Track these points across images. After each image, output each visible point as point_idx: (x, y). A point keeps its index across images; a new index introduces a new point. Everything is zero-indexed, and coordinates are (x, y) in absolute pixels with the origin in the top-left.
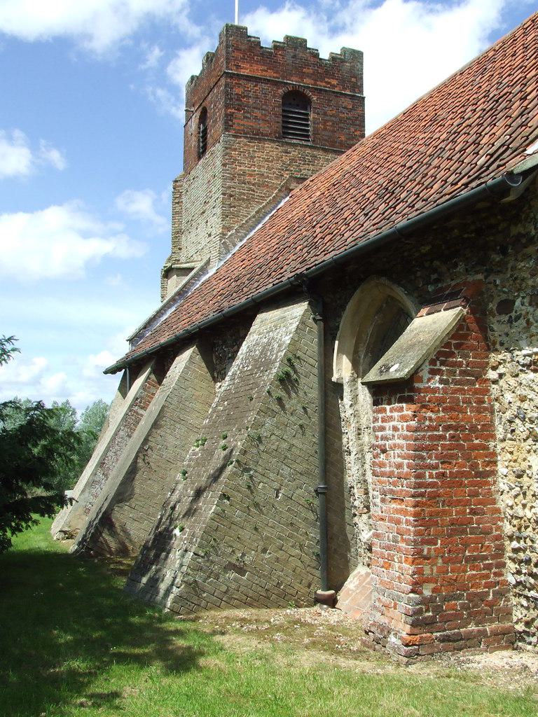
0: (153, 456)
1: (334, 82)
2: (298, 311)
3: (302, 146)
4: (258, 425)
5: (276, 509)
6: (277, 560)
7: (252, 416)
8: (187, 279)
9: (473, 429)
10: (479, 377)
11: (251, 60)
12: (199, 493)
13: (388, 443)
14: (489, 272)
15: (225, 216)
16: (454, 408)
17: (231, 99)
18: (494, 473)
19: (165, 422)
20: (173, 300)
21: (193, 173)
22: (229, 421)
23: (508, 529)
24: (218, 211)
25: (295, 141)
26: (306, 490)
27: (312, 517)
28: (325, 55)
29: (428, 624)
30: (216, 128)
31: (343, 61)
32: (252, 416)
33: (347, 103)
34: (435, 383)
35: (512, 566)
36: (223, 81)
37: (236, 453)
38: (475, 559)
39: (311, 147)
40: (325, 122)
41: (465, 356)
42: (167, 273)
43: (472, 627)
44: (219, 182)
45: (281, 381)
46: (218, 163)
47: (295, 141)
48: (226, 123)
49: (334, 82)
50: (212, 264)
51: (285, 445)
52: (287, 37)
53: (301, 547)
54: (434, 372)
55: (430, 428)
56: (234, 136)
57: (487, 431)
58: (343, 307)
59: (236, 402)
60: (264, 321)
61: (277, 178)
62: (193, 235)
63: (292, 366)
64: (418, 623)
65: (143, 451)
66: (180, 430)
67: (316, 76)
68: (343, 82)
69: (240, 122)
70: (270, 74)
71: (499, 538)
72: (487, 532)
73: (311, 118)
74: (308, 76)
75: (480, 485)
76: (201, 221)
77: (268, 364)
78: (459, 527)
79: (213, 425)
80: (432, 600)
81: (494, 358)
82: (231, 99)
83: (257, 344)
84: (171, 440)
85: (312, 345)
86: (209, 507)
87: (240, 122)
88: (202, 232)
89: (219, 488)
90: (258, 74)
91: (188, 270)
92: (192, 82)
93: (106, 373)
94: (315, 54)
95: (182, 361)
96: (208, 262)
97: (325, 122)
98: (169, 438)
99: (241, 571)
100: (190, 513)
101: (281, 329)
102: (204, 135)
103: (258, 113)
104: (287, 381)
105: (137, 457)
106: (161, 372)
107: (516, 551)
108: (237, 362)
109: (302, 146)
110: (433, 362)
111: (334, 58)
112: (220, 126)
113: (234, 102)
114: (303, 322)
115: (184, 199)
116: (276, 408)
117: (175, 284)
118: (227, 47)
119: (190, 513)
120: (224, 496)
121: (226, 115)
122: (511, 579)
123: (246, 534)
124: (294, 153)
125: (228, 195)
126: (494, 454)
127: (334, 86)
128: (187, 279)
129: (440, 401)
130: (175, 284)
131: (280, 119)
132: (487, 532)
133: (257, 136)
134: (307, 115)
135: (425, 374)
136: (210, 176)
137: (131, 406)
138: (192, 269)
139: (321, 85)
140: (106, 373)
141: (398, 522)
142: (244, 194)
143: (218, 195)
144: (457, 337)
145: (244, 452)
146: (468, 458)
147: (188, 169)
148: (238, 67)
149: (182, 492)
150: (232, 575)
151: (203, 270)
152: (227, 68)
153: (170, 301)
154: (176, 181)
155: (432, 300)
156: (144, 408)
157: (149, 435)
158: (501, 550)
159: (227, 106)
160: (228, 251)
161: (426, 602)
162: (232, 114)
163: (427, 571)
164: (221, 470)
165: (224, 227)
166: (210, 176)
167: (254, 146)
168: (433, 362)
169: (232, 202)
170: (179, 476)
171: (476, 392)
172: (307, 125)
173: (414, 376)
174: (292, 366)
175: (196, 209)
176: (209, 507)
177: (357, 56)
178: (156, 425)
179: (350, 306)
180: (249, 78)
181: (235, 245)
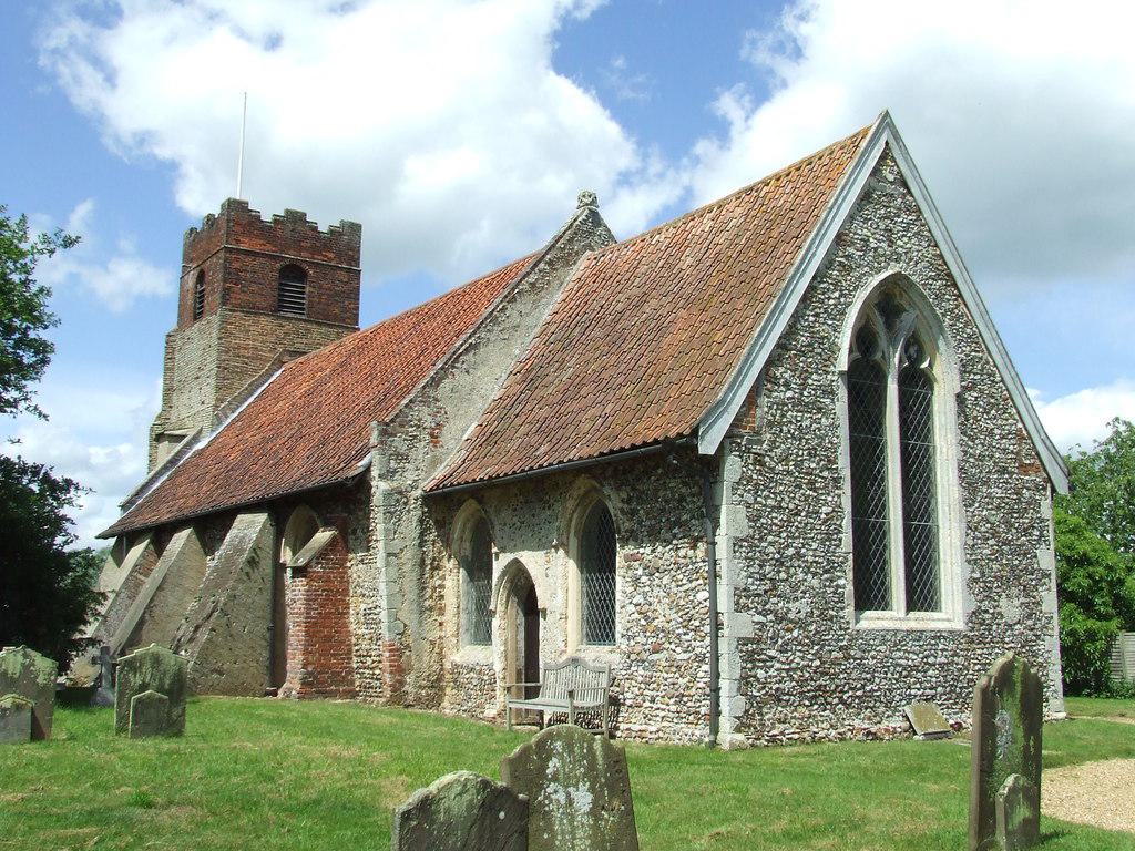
0: (157, 611)
1: (332, 255)
2: (262, 518)
3: (296, 319)
4: (234, 588)
6: (243, 668)
7: (231, 583)
8: (179, 446)
9: (338, 591)
10: (342, 566)
11: (250, 235)
12: (197, 628)
13: (297, 598)
14: (350, 513)
15: (219, 388)
16: (328, 580)
17: (230, 273)
18: (348, 613)
19: (167, 586)
20: (165, 468)
21: (187, 332)
22: (217, 586)
23: (354, 640)
24: (212, 382)
25: (289, 315)
26: (262, 627)
27: (266, 644)
28: (323, 228)
29: (310, 684)
30: (214, 298)
31: (341, 234)
32: (231, 583)
33: (344, 276)
34: (319, 568)
35: (355, 659)
36: (222, 254)
37: (221, 605)
38: (337, 654)
39: (305, 321)
40: (320, 295)
41: (335, 555)
42: (159, 438)
43: (333, 688)
44: (214, 354)
45: (249, 562)
46: (215, 334)
47: (289, 315)
48: (223, 297)
49: (332, 255)
50: (204, 434)
51: (250, 601)
52: (287, 211)
53: (257, 662)
54: (318, 563)
55: (315, 590)
56: (230, 310)
57: (346, 592)
58: (288, 517)
59: (222, 572)
60: (242, 520)
61: (270, 351)
62: (185, 396)
63: (256, 553)
64: (304, 683)
65: (149, 608)
66: (178, 592)
67: (314, 250)
68: (339, 256)
69: (238, 296)
70: (268, 249)
71: (348, 645)
72: (343, 642)
73: (307, 290)
74: (306, 249)
75: (340, 619)
78: (328, 638)
79: (207, 588)
80: (312, 673)
81: (351, 556)
82: (230, 273)
83: (237, 537)
84: (171, 600)
85: (269, 540)
86: (203, 636)
87: (238, 296)
88: (195, 397)
89: (210, 625)
90: (257, 249)
91: (180, 438)
92: (190, 234)
93: (97, 538)
95: (181, 539)
96: (200, 432)
97: (320, 295)
98: (170, 598)
99: (221, 673)
100: (191, 640)
101: (249, 528)
102: (200, 297)
103: (254, 287)
104: (252, 562)
105: (144, 613)
106: (159, 544)
107: (357, 651)
108: (223, 547)
109: (296, 319)
110: (318, 558)
112: (217, 297)
113: (231, 276)
114: (264, 526)
115: (177, 356)
116: (245, 578)
117: (166, 451)
118: (228, 221)
119: (191, 640)
120: (213, 630)
121: (224, 289)
122: (355, 666)
123: (225, 652)
124: (288, 326)
125: (222, 368)
126: (348, 604)
127: (330, 260)
128: (179, 446)
129: (321, 577)
130: (166, 451)
131: (276, 294)
132: (343, 642)
133: (253, 310)
134: (304, 288)
135: (313, 564)
136: (204, 339)
138: (184, 436)
139: (318, 259)
140: (97, 538)
141: (298, 636)
142: (238, 367)
143: (212, 367)
144: (331, 545)
145: (225, 604)
146: (334, 605)
147: (182, 324)
148: (238, 241)
149: (186, 629)
150: (215, 676)
151: (196, 439)
152: (227, 242)
153: (162, 468)
154: (169, 336)
155: (327, 524)
156: (147, 576)
157: (154, 596)
158: (350, 652)
159: (225, 281)
160: (220, 423)
161: (308, 673)
162: (229, 289)
163: (310, 659)
164: (212, 612)
165: (217, 399)
166: (204, 339)
168: (318, 558)
169: (227, 376)
170: (183, 621)
171: (341, 573)
172: (303, 298)
173: (308, 565)
174: (256, 553)
175: (190, 371)
176: (203, 636)
177: (355, 229)
178: (160, 588)
179: (294, 514)
180: (247, 253)
181: (227, 417)
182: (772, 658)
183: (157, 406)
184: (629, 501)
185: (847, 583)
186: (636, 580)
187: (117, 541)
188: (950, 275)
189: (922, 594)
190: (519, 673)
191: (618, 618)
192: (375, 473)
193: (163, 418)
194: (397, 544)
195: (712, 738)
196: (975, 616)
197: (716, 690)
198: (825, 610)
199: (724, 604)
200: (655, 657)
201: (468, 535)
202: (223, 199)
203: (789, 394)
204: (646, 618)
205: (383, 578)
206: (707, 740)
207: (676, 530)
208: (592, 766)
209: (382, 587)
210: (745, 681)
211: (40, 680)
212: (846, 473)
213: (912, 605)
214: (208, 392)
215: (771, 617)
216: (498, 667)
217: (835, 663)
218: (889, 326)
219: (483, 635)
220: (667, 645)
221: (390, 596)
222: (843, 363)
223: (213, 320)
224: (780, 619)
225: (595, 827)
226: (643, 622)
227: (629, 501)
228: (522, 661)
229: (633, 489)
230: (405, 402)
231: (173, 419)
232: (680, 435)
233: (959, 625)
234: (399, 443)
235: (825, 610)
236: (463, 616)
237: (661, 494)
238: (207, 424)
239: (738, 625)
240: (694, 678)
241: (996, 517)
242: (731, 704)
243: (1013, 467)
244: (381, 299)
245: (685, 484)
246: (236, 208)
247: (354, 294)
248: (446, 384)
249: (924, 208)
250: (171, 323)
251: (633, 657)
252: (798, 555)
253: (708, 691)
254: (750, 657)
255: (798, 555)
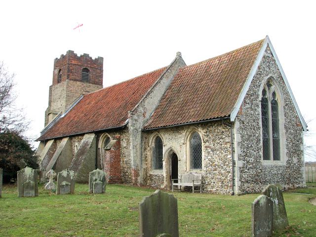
5: (209, 233)
15: (66, 101)
28: (93, 59)
46: (65, 86)
60: (86, 136)
68: (98, 66)
69: (72, 77)
70: (79, 64)
76: (59, 101)
77: (88, 145)
87: (72, 77)
90: (76, 64)
94: (91, 58)
101: (89, 138)
111: (96, 59)
112: (66, 76)
113: (69, 71)
115: (53, 92)
124: (85, 85)
130: (51, 118)
133: (76, 80)
137: (54, 153)
167: (75, 83)
177: (102, 59)
182: (246, 172)
183: (47, 106)
184: (206, 133)
185: (261, 153)
186: (209, 153)
187: (54, 142)
188: (282, 77)
189: (277, 157)
190: (170, 177)
191: (203, 162)
192: (130, 124)
193: (49, 109)
194: (136, 143)
195: (232, 192)
196: (288, 162)
197: (234, 180)
198: (257, 158)
199: (236, 159)
200: (215, 172)
201: (154, 141)
202: (67, 50)
203: (249, 106)
204: (212, 162)
205: (132, 152)
206: (231, 192)
207: (221, 140)
208: (277, 195)
209: (132, 155)
210: (241, 177)
211: (72, 178)
212: (261, 126)
213: (274, 159)
214: (63, 102)
215: (246, 162)
216: (165, 175)
217: (259, 173)
218: (269, 89)
219: (160, 167)
220: (218, 169)
221: (134, 157)
222: (260, 99)
223: (65, 83)
224: (248, 162)
225: (279, 207)
226: (211, 163)
227: (206, 133)
228: (171, 173)
229: (208, 129)
230: (136, 106)
231: (52, 109)
232: (225, 116)
233: (285, 164)
234: (135, 117)
235: (257, 161)
236: (153, 163)
237: (216, 131)
238: (63, 111)
239: (239, 164)
240: (227, 177)
241: (292, 137)
242: (237, 183)
243: (295, 125)
244: (111, 78)
245: (223, 128)
246: (71, 53)
247: (101, 76)
248: (147, 101)
249: (276, 60)
250: (51, 84)
251: (208, 172)
252: (251, 146)
253: (231, 180)
254: (241, 172)
255: (251, 146)
